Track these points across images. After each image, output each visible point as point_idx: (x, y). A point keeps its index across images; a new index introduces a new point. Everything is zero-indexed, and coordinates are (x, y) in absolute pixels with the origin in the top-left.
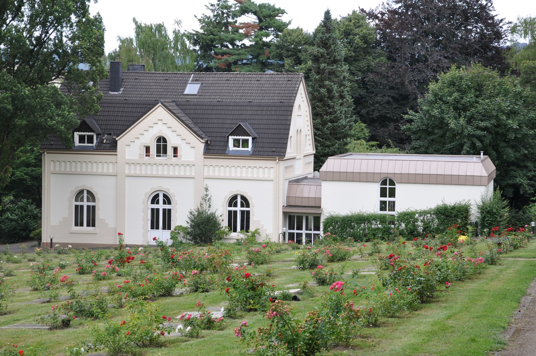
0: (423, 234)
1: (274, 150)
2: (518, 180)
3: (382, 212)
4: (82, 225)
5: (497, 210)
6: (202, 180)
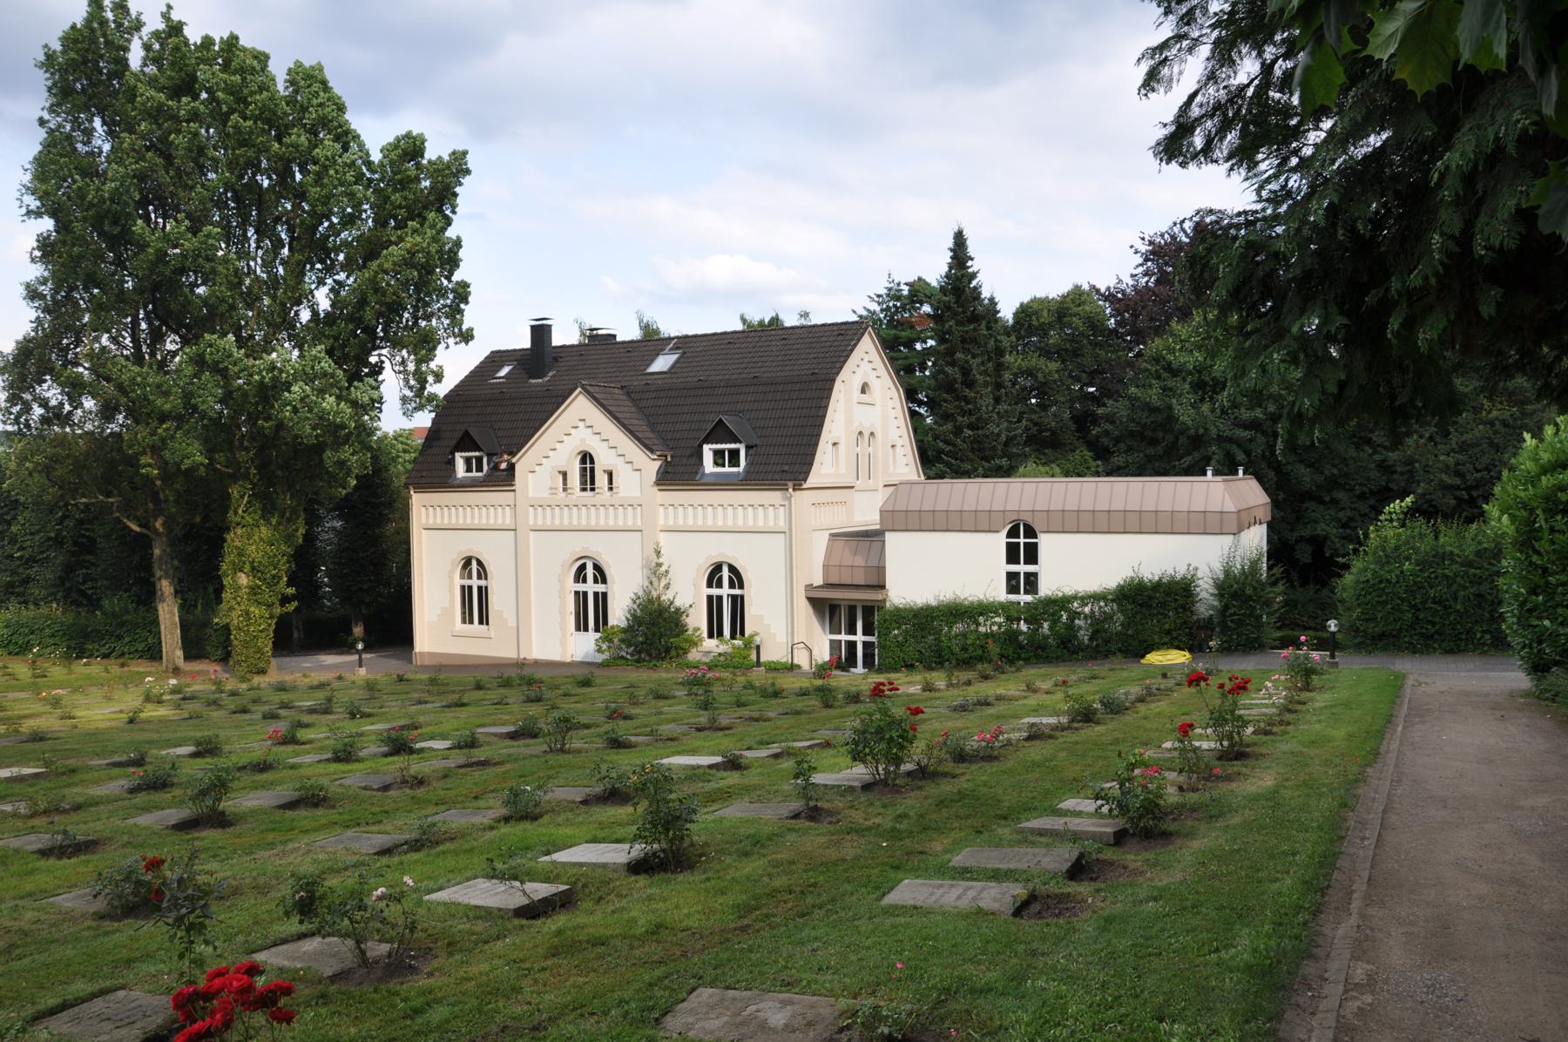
2: (1322, 528)
3: (1013, 597)
4: (471, 622)
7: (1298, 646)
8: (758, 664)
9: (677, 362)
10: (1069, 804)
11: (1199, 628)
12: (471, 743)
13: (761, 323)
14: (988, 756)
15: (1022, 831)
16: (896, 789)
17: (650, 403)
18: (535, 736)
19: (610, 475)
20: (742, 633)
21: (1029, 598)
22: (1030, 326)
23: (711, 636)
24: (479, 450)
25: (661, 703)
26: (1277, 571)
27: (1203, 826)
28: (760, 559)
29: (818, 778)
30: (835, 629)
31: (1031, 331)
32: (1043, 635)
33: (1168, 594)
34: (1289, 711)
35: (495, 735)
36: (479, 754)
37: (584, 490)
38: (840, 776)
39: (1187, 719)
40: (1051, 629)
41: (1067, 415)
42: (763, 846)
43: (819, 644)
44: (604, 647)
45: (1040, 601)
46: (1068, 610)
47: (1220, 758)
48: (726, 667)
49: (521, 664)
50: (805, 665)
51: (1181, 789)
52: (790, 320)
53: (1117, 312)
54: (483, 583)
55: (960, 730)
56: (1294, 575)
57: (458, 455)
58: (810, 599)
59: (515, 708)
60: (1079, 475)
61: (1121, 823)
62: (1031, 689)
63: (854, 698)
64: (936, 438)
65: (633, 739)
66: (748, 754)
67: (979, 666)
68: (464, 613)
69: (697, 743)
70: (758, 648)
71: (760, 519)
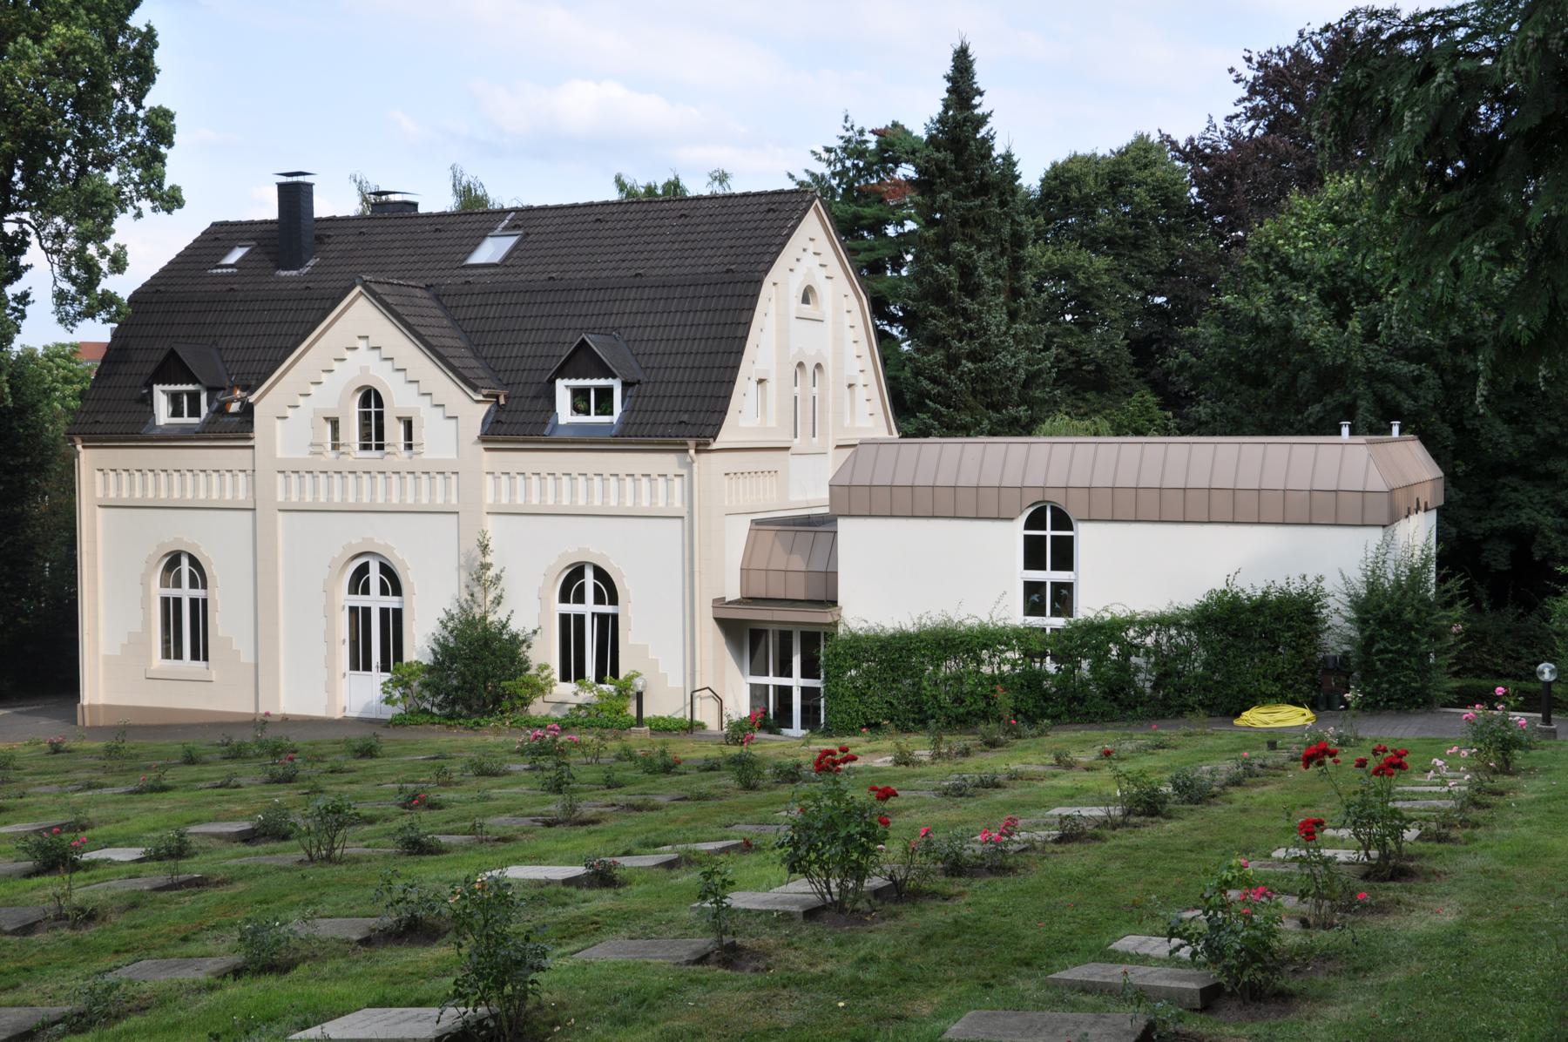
0: (1151, 698)
1: (685, 417)
2: (1525, 517)
3: (1035, 621)
4: (179, 656)
5: (1418, 612)
6: (505, 523)
7: (1490, 700)
8: (640, 720)
9: (515, 248)
10: (1129, 943)
11: (1326, 671)
12: (178, 851)
13: (650, 190)
14: (997, 866)
15: (1056, 984)
16: (858, 918)
17: (472, 313)
18: (285, 837)
19: (408, 424)
20: (615, 673)
21: (1059, 622)
22: (1067, 200)
23: (565, 677)
24: (194, 381)
25: (486, 782)
26: (1455, 584)
27: (1343, 985)
28: (648, 556)
29: (738, 900)
30: (758, 669)
31: (1067, 207)
32: (1083, 679)
33: (1278, 619)
34: (1477, 805)
35: (218, 836)
36: (192, 868)
37: (365, 447)
38: (770, 895)
39: (1312, 813)
40: (1093, 669)
41: (1120, 341)
42: (651, 1007)
43: (734, 690)
44: (397, 695)
45: (1076, 627)
46: (1120, 642)
47: (1366, 877)
48: (590, 726)
49: (262, 723)
50: (712, 724)
51: (1304, 923)
52: (697, 186)
53: (1199, 179)
54: (199, 593)
55: (954, 825)
56: (1482, 591)
57: (158, 389)
58: (723, 623)
59: (251, 792)
60: (1138, 432)
61: (1213, 975)
62: (1064, 763)
63: (790, 775)
64: (917, 373)
65: (443, 839)
66: (626, 861)
67: (982, 727)
68: (166, 642)
69: (544, 845)
70: (639, 696)
71: (644, 497)
